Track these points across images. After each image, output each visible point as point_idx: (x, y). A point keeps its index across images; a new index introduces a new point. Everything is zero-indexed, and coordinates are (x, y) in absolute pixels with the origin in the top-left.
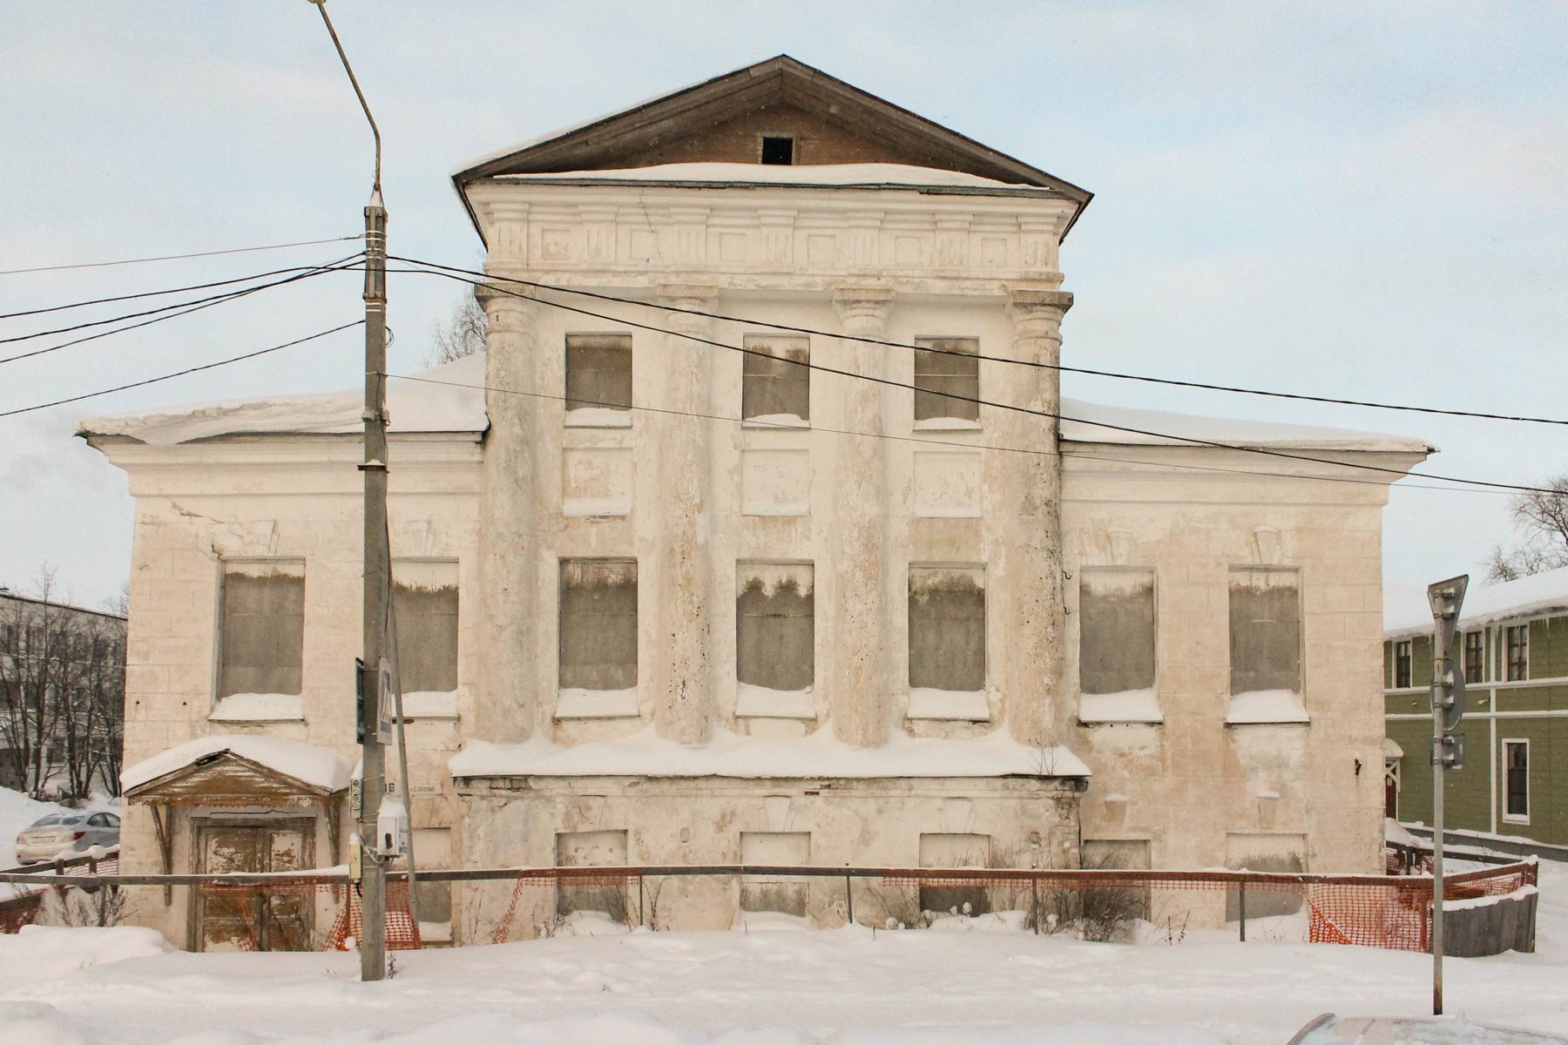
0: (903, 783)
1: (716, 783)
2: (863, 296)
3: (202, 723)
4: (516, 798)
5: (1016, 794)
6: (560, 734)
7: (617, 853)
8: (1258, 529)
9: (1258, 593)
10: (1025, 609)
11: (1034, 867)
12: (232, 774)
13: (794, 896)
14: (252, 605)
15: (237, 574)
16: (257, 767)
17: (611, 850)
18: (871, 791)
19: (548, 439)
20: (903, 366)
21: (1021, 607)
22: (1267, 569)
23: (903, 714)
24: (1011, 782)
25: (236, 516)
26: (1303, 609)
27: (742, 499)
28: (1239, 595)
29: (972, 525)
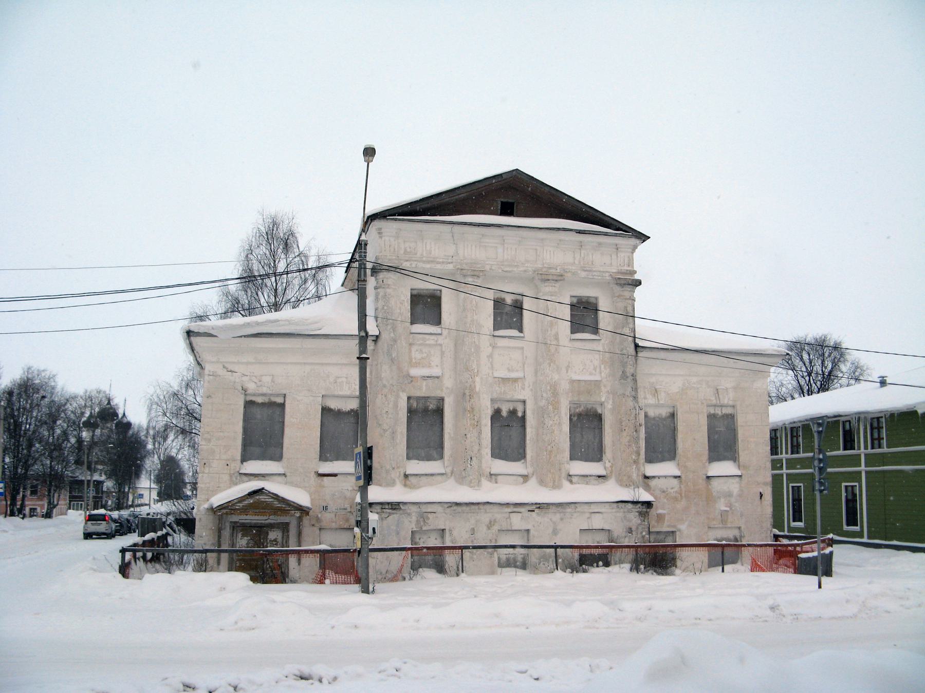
0: (573, 505)
1: (487, 507)
2: (550, 277)
3: (236, 475)
4: (393, 514)
5: (622, 510)
6: (408, 482)
7: (439, 540)
8: (718, 388)
10: (623, 424)
11: (636, 543)
12: (263, 500)
13: (521, 560)
14: (259, 416)
15: (251, 401)
16: (276, 497)
17: (436, 539)
18: (558, 509)
19: (403, 339)
20: (566, 312)
21: (621, 423)
22: (722, 406)
23: (567, 473)
24: (620, 505)
25: (253, 373)
26: (737, 424)
27: (493, 370)
28: (711, 417)
29: (597, 384)
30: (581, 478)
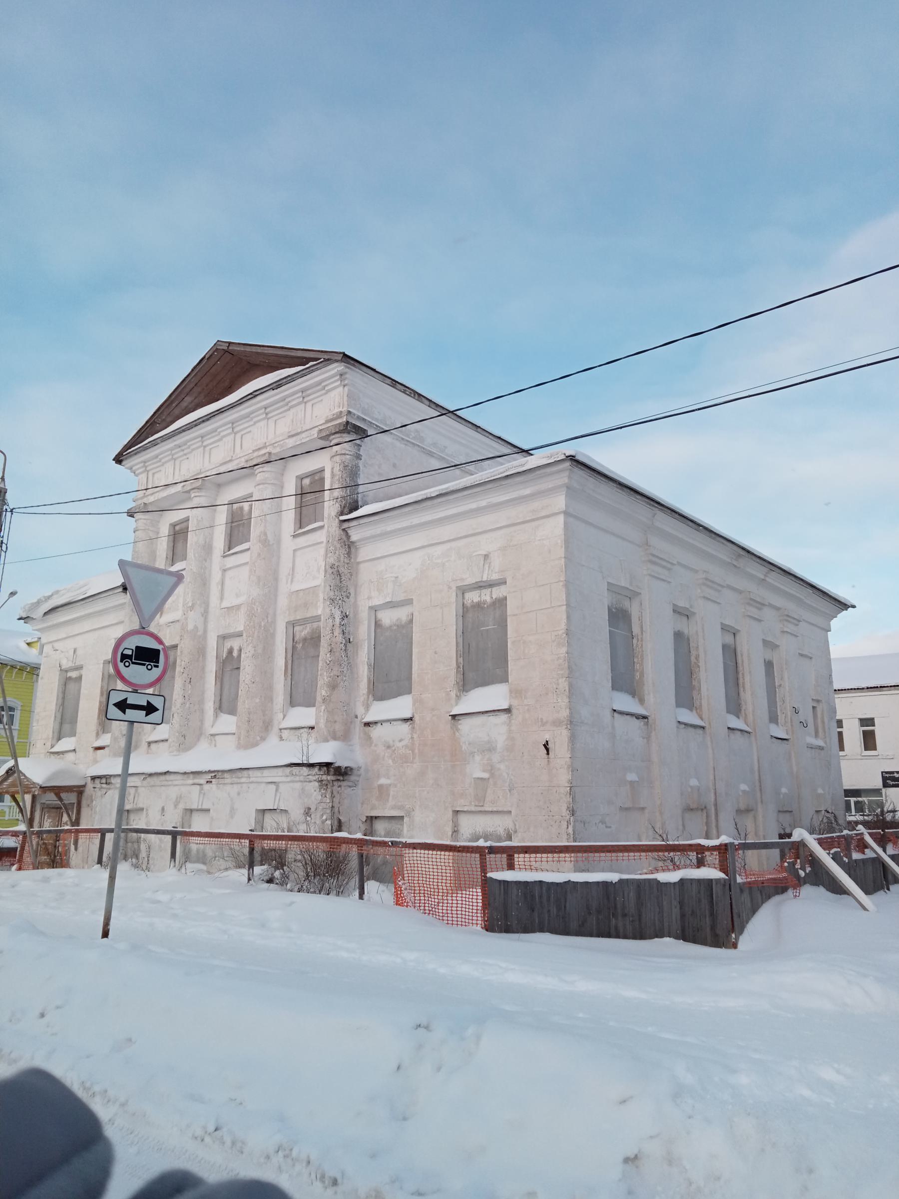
9: (485, 606)
24: (296, 770)
30: (293, 731)
